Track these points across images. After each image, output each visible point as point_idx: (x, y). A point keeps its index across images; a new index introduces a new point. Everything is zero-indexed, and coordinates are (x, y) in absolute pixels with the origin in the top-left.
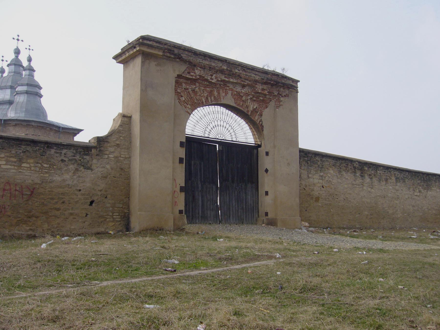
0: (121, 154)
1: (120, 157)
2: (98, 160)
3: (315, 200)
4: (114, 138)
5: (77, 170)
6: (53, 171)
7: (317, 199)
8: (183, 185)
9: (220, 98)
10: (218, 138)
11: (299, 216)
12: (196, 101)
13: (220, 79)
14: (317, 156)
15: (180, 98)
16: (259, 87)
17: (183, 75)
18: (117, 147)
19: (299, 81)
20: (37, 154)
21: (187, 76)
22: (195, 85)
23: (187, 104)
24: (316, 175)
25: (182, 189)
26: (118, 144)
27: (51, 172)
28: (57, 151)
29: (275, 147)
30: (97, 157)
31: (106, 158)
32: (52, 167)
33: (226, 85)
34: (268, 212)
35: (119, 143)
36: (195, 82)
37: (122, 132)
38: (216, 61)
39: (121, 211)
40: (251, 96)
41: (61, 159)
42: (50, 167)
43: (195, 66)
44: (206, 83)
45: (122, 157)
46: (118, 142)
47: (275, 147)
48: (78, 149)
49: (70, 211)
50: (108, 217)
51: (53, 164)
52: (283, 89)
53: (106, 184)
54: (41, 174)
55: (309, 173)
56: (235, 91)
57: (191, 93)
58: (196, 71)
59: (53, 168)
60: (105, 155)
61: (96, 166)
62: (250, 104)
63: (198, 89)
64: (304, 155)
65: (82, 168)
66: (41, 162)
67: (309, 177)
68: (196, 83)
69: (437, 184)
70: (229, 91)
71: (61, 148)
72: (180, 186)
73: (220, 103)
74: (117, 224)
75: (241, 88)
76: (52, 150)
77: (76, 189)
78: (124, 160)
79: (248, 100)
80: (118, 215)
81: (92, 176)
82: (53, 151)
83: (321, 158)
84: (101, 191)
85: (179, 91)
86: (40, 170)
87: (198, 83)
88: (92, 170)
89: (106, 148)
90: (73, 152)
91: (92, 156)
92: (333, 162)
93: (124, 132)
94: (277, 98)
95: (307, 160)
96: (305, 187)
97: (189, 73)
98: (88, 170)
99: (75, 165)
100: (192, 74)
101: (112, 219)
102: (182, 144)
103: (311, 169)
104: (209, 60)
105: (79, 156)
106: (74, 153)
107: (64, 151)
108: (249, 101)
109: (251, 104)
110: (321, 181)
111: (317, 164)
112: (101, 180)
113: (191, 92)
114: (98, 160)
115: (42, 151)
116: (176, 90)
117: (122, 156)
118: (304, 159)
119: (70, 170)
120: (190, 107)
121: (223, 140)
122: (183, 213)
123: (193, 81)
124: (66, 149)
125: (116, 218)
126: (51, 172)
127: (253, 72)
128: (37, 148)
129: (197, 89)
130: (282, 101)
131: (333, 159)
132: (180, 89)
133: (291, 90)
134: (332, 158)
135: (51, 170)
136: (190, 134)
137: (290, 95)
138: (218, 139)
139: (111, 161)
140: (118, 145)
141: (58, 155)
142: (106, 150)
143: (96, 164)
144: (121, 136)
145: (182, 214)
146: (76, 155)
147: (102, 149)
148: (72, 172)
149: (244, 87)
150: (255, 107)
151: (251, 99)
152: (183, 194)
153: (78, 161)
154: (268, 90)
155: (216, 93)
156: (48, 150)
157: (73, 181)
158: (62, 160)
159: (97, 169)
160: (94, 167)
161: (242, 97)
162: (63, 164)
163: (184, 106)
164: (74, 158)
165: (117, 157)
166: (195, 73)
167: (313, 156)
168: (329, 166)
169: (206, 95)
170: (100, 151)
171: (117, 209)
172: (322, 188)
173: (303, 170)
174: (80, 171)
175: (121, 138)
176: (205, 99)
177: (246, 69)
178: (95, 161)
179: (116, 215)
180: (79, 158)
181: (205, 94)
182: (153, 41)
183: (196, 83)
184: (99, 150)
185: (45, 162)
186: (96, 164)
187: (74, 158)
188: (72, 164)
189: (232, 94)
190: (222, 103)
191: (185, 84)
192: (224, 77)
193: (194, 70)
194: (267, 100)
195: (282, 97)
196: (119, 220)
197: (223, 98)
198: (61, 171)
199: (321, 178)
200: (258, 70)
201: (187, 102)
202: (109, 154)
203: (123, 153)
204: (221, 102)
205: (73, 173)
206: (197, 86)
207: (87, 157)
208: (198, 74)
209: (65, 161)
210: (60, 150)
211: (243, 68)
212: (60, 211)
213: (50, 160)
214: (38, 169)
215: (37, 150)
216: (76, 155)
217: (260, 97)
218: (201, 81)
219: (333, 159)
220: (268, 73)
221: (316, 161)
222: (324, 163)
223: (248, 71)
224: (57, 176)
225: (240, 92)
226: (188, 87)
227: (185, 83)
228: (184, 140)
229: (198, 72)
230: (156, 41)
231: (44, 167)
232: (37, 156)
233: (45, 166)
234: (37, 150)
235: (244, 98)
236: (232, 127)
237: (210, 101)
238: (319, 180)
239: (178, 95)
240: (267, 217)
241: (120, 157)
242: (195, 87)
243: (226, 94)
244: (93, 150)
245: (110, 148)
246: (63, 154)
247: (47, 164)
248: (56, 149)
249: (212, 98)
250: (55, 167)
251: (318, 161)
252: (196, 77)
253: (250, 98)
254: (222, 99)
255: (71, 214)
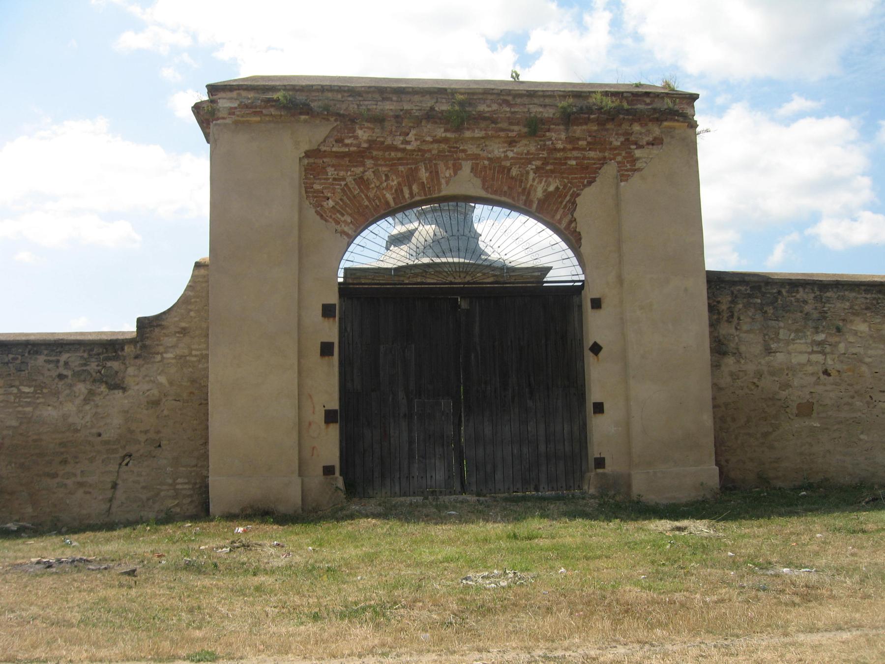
0: (192, 350)
1: (190, 355)
2: (139, 368)
3: (795, 411)
4: (175, 317)
5: (91, 393)
6: (41, 400)
7: (806, 410)
8: (335, 405)
9: (439, 184)
10: (453, 280)
11: (714, 462)
12: (367, 203)
13: (429, 139)
14: (801, 290)
15: (323, 203)
16: (558, 137)
17: (323, 148)
18: (182, 335)
19: (698, 95)
20: (9, 368)
21: (334, 149)
22: (363, 164)
23: (343, 215)
24: (798, 341)
25: (330, 417)
26: (184, 329)
27: (38, 401)
28: (49, 358)
29: (620, 280)
30: (136, 360)
31: (158, 362)
32: (38, 391)
33: (457, 147)
34: (604, 458)
35: (187, 326)
36: (363, 157)
37: (193, 300)
38: (417, 98)
39: (193, 474)
40: (539, 163)
41: (57, 373)
42: (35, 392)
43: (353, 121)
44: (393, 154)
45: (193, 356)
46: (183, 325)
47: (620, 280)
48: (92, 350)
49: (79, 479)
50: (164, 487)
51: (41, 384)
52: (641, 125)
53: (158, 417)
54: (18, 407)
55: (772, 339)
56: (484, 159)
57: (351, 186)
58: (360, 133)
59: (42, 393)
60: (156, 356)
61: (134, 381)
62: (536, 182)
63: (372, 175)
64: (748, 291)
65: (103, 388)
66: (17, 383)
67: (771, 349)
68: (366, 160)
69: (782, 334)
70: (463, 163)
71: (57, 352)
72: (326, 408)
73: (436, 195)
74: (184, 501)
75: (503, 147)
76: (38, 357)
77: (90, 433)
78: (199, 361)
79: (528, 173)
80: (186, 483)
81: (126, 401)
82: (41, 359)
83: (818, 293)
84: (146, 432)
85: (317, 187)
86: (17, 400)
87: (368, 158)
88: (124, 389)
89: (157, 340)
90: (82, 357)
91: (124, 360)
92: (866, 298)
93: (198, 300)
94: (624, 154)
95: (761, 304)
96: (755, 380)
97: (339, 141)
98: (116, 392)
99: (88, 383)
100: (347, 141)
101: (171, 493)
102: (328, 311)
103: (780, 328)
104: (394, 98)
105: (96, 363)
106: (85, 359)
107: (64, 357)
108: (532, 175)
109: (540, 182)
110: (819, 358)
111: (801, 312)
112: (147, 409)
113: (352, 185)
114: (139, 368)
115: (18, 362)
116: (308, 188)
117: (194, 353)
118: (751, 301)
119: (77, 395)
120: (349, 219)
121: (468, 283)
122: (334, 474)
123: (359, 156)
124: (68, 352)
125: (182, 489)
126: (38, 401)
127: (536, 101)
128: (11, 356)
129: (369, 174)
130: (638, 159)
131: (867, 291)
132: (323, 181)
133: (666, 124)
134: (863, 288)
135: (38, 398)
136: (369, 281)
137: (666, 140)
138: (451, 283)
139: (169, 366)
140: (184, 331)
141: (51, 366)
142: (158, 345)
143: (134, 376)
144: (191, 310)
145: (332, 476)
146: (89, 363)
147: (148, 342)
148: (82, 397)
149: (514, 144)
150: (551, 188)
151: (537, 170)
152: (334, 431)
153: (94, 374)
154: (589, 139)
155: (423, 174)
156: (31, 358)
157: (83, 417)
158: (61, 377)
159: (136, 388)
160: (129, 381)
161: (509, 170)
162: (63, 382)
163: (334, 219)
164: (85, 368)
165: (182, 356)
166: (356, 138)
167: (784, 291)
168: (850, 311)
169: (395, 182)
170: (144, 347)
171: (184, 469)
172: (823, 377)
173: (747, 332)
174: (100, 395)
175: (192, 314)
176: (392, 194)
177: (510, 98)
178: (131, 371)
179: (182, 484)
180: (96, 368)
181: (393, 181)
182: (239, 89)
183: (366, 160)
184: (141, 347)
185: (25, 383)
186: (134, 376)
187: (85, 368)
188: (80, 381)
189: (473, 169)
190: (443, 193)
191: (333, 169)
192: (442, 130)
193: (354, 131)
194: (594, 164)
195: (640, 147)
196: (189, 493)
197: (447, 183)
198: (58, 398)
199: (819, 349)
200: (548, 94)
201: (342, 208)
202: (166, 352)
203: (195, 346)
204: (440, 191)
205: (85, 400)
206: (368, 166)
207: (115, 365)
208: (365, 138)
209: (66, 377)
210: (55, 356)
211: (502, 97)
212: (59, 480)
213: (35, 378)
214: (12, 398)
215: (9, 361)
216: (89, 363)
217: (570, 159)
218: (380, 153)
219: (865, 290)
220: (583, 94)
221: (795, 304)
222: (827, 305)
223: (518, 101)
224: (50, 408)
225: (500, 158)
226: (342, 173)
227: (333, 166)
228: (333, 298)
229: (363, 134)
230: (245, 87)
231: (24, 392)
232: (10, 373)
233: (26, 390)
234: (9, 361)
235: (514, 172)
236: (496, 247)
237: (407, 196)
238: (811, 356)
239: (316, 197)
240: (600, 471)
241: (190, 355)
242: (361, 169)
243: (457, 168)
244: (126, 348)
245: (166, 339)
246: (62, 363)
247: (30, 387)
248: (47, 355)
249: (415, 188)
250: (45, 391)
251: (805, 302)
252: (359, 146)
253: (534, 167)
254: (443, 186)
255: (81, 484)
